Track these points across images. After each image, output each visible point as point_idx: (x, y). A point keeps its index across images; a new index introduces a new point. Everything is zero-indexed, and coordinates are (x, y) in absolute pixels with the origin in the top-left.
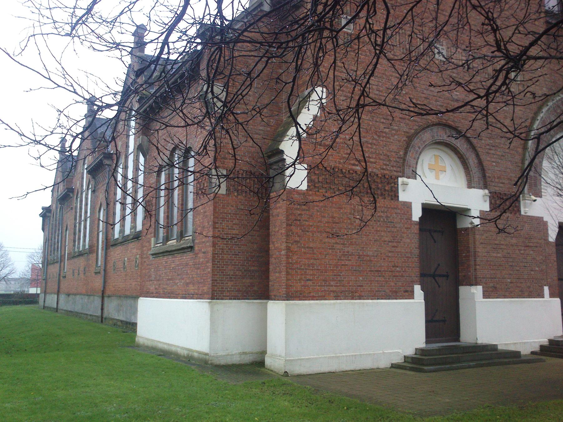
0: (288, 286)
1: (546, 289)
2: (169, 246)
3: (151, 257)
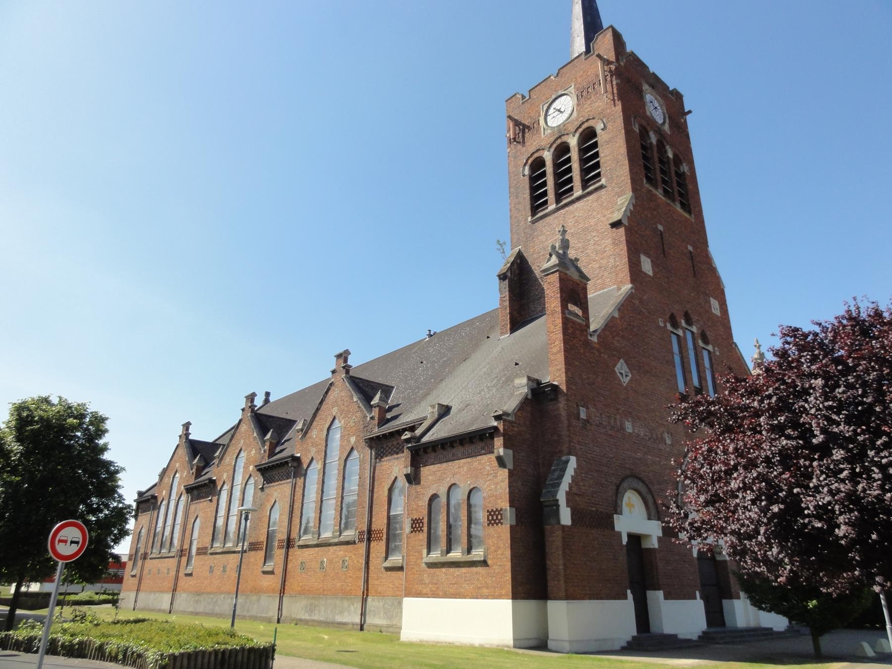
1: (698, 593)
3: (424, 565)
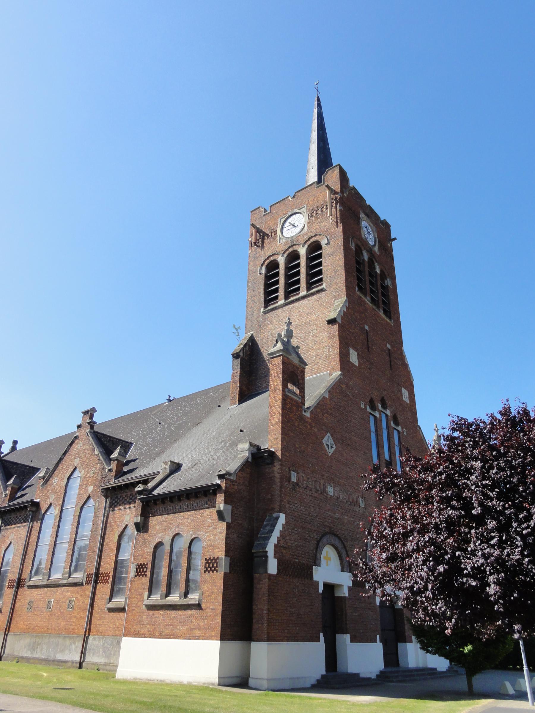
0: (268, 633)
2: (168, 601)
3: (144, 607)
